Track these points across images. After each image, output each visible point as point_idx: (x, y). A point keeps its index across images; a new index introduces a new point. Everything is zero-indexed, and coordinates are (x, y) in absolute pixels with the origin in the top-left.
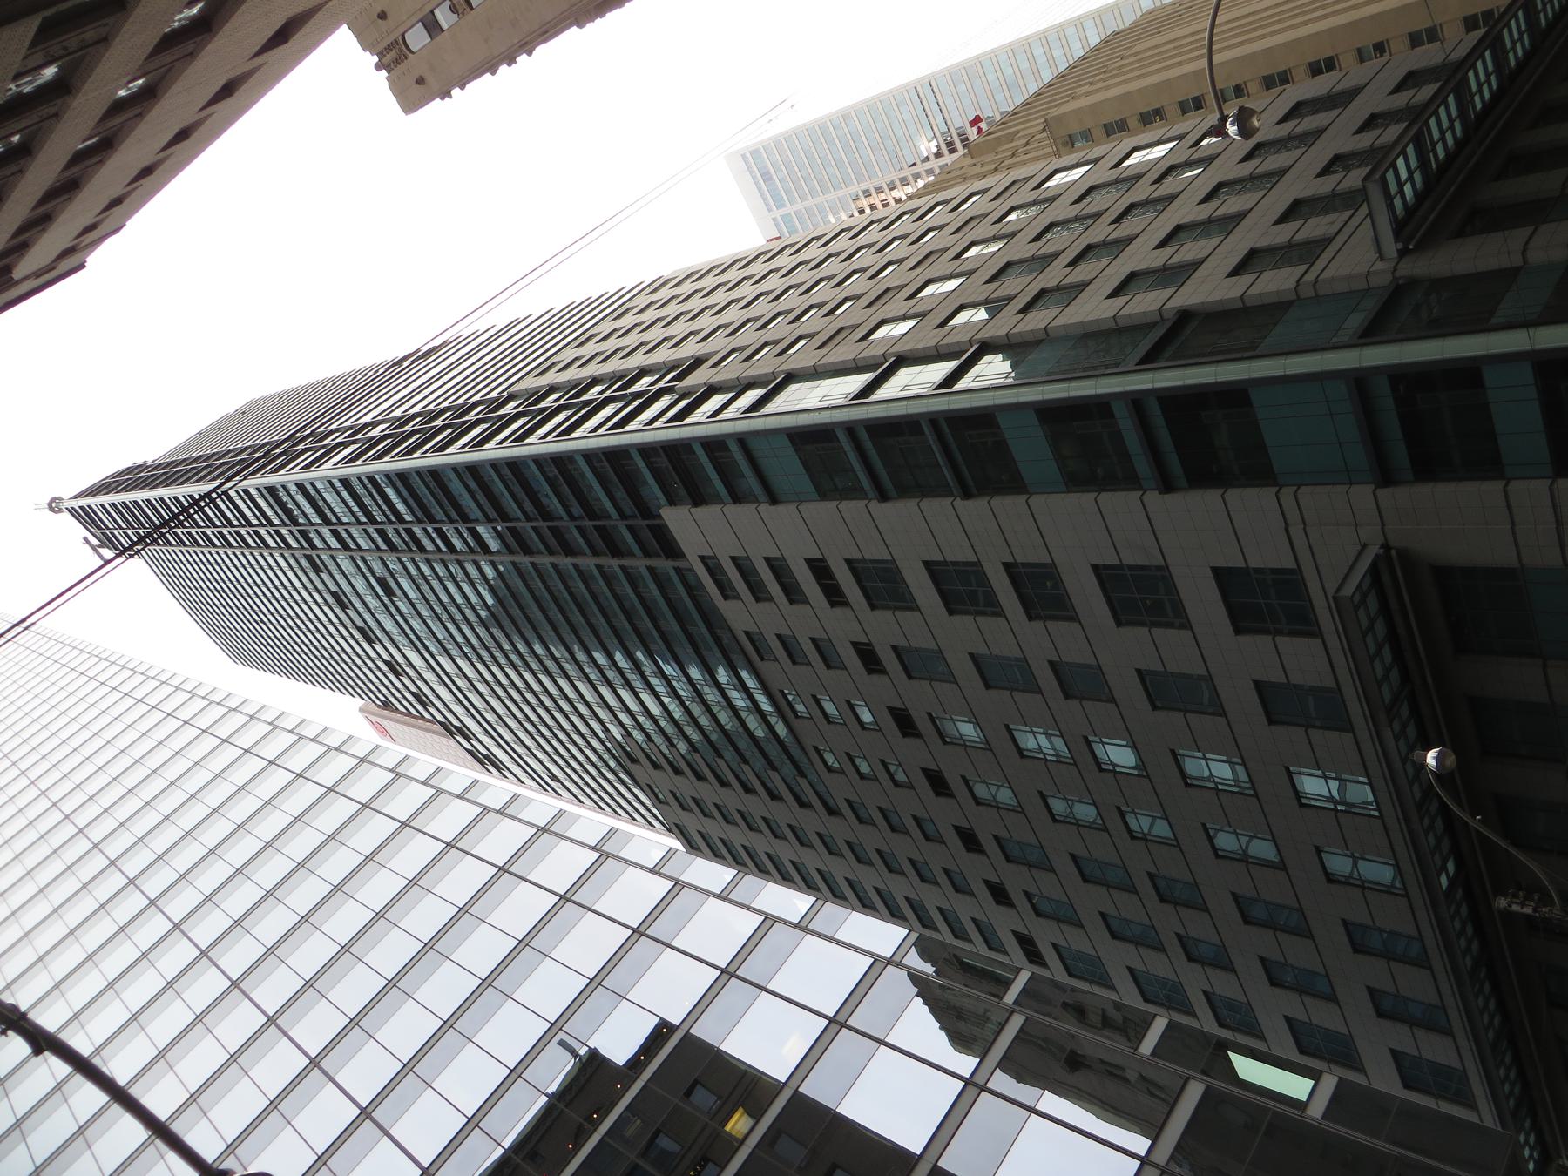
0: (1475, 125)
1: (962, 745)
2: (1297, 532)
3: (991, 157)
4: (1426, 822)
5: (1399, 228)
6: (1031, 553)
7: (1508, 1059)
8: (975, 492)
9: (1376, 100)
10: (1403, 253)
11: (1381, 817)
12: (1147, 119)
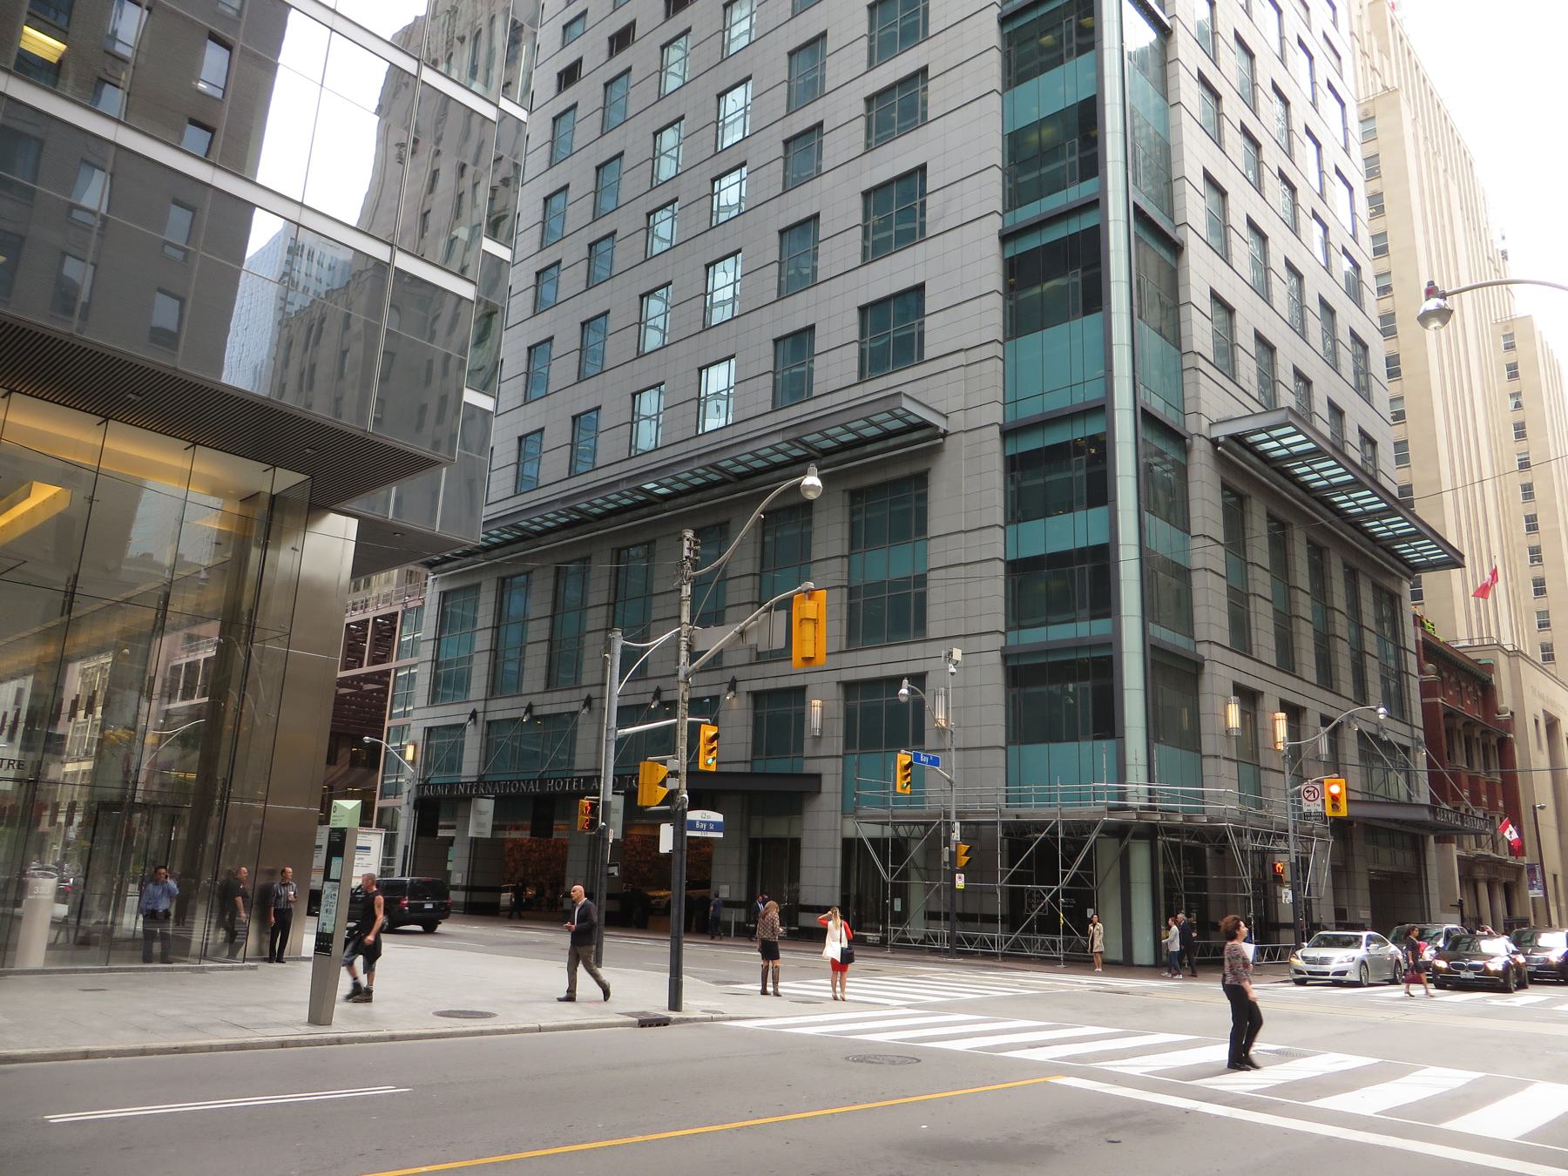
0: (1320, 498)
1: (724, 26)
2: (960, 359)
3: (1366, 27)
4: (700, 471)
5: (1238, 438)
6: (937, 96)
7: (506, 536)
8: (1007, 30)
9: (1357, 414)
10: (1215, 442)
11: (698, 436)
12: (1377, 204)
